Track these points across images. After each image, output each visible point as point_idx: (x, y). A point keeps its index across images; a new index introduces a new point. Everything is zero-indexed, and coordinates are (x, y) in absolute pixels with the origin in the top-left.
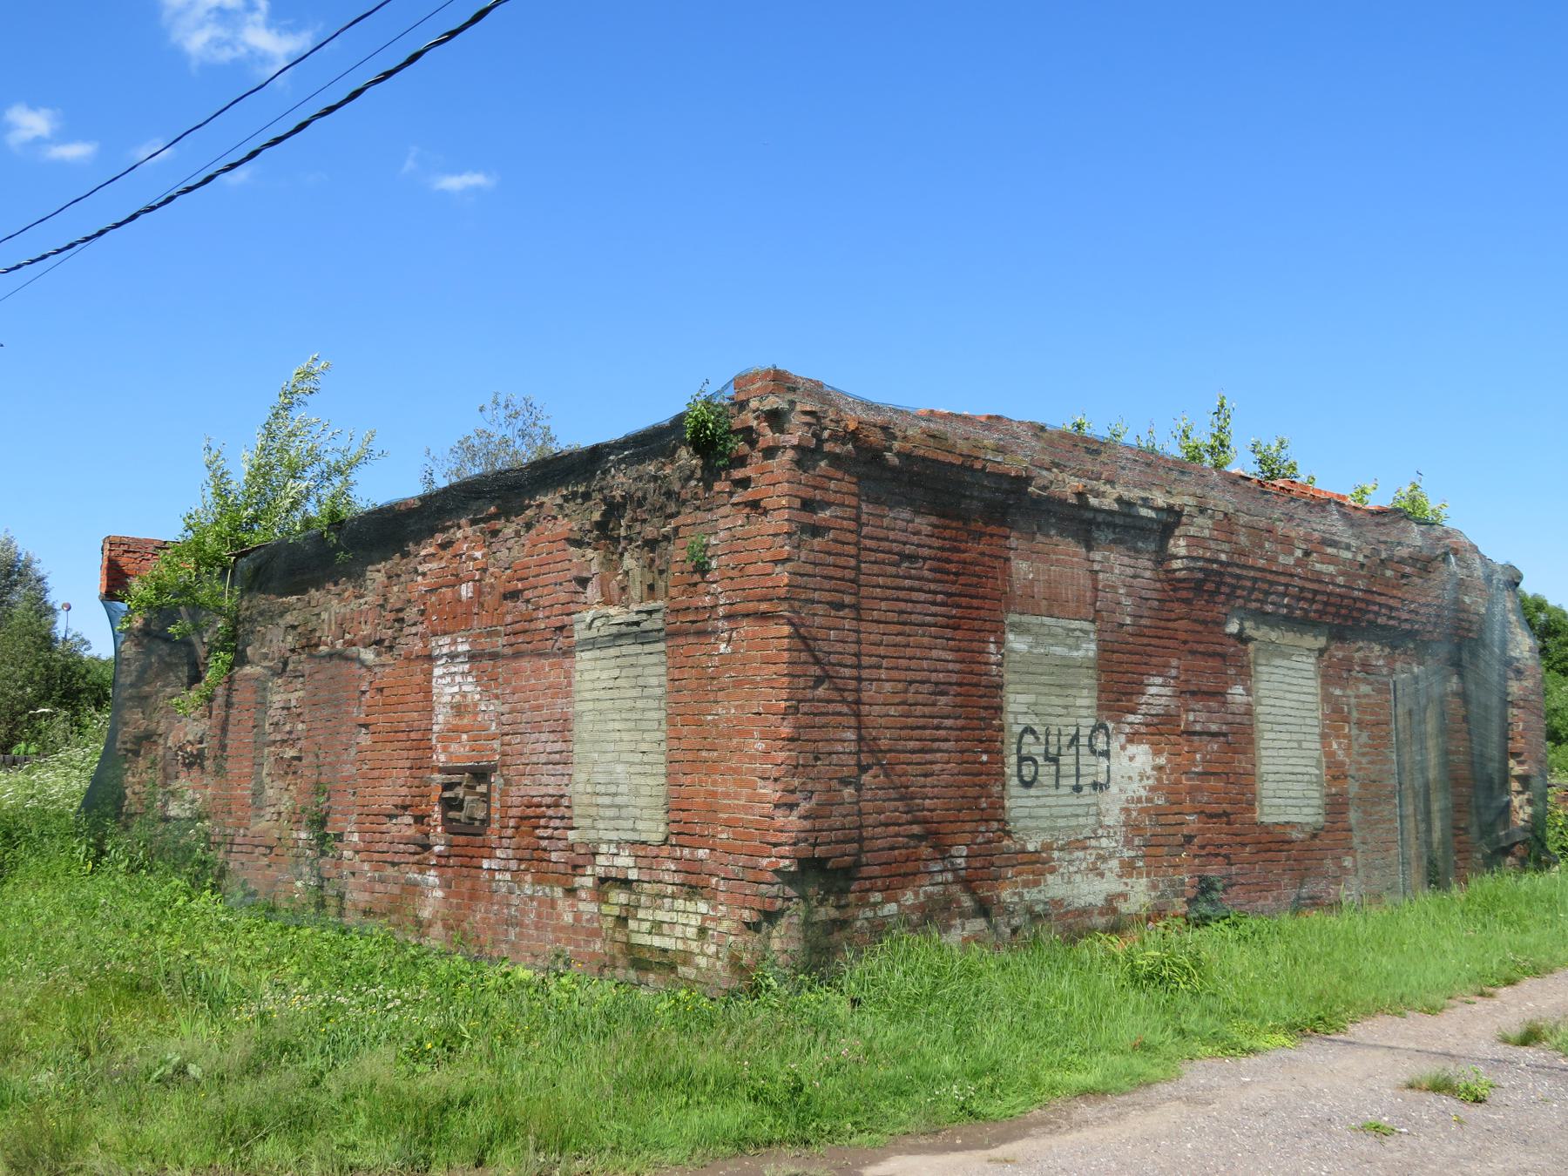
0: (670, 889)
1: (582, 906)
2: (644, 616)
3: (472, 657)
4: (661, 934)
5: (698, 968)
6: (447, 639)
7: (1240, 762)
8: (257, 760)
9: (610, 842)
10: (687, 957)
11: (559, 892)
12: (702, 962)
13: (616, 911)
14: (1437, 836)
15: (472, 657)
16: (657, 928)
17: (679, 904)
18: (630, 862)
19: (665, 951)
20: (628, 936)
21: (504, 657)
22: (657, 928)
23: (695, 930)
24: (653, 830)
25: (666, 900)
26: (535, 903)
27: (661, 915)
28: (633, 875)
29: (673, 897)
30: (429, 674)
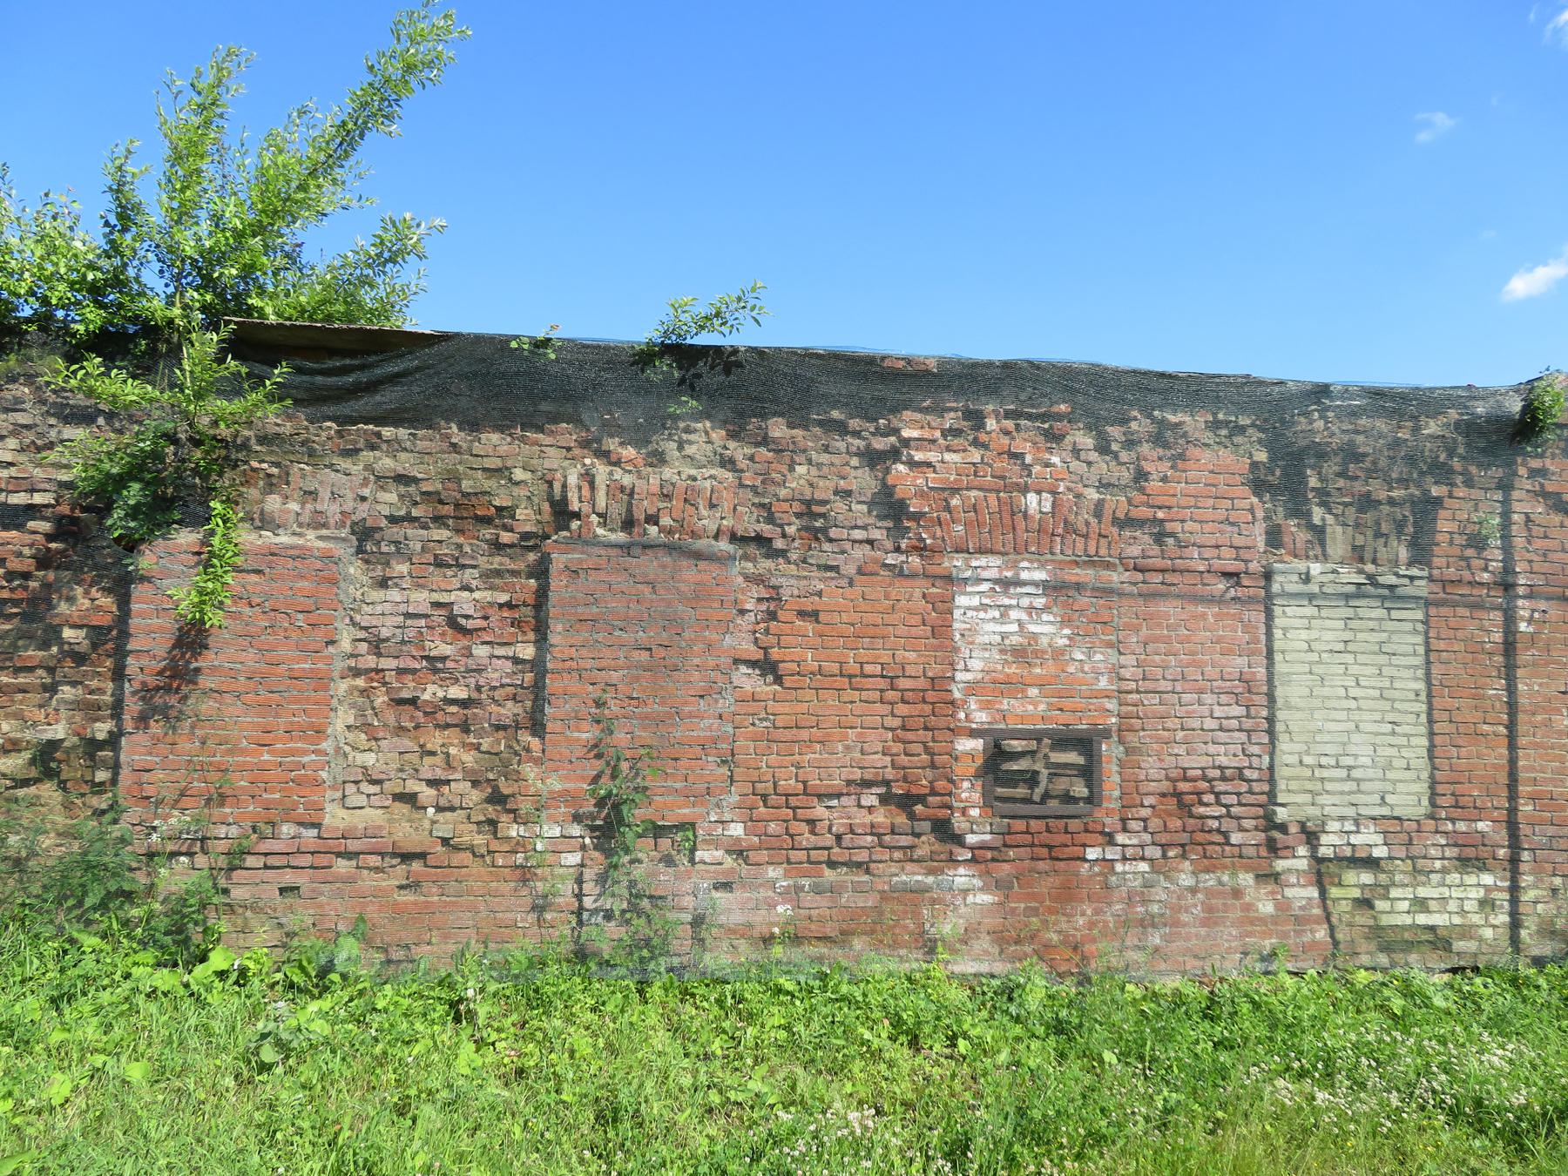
0: (1438, 864)
1: (1289, 892)
2: (1406, 581)
3: (1053, 589)
4: (1428, 911)
5: (1481, 940)
6: (995, 561)
7: (367, 293)
8: (1197, 1074)
9: (1342, 818)
10: (1467, 932)
11: (1246, 879)
12: (1488, 933)
13: (1356, 893)
14: (1414, 606)
15: (1053, 589)
16: (1421, 904)
17: (1455, 877)
18: (1379, 839)
19: (1432, 928)
20: (1375, 918)
21: (1121, 594)
22: (1421, 904)
23: (1475, 903)
24: (1410, 799)
25: (1432, 876)
26: (1200, 896)
27: (1422, 892)
28: (1380, 852)
29: (1444, 871)
30: (944, 607)
